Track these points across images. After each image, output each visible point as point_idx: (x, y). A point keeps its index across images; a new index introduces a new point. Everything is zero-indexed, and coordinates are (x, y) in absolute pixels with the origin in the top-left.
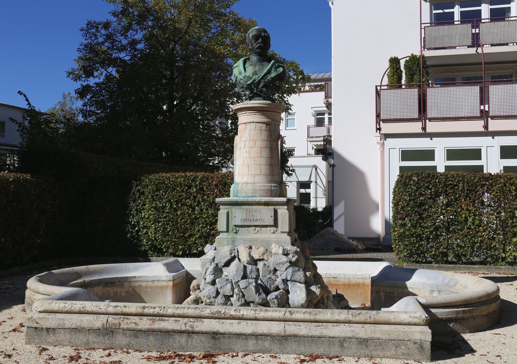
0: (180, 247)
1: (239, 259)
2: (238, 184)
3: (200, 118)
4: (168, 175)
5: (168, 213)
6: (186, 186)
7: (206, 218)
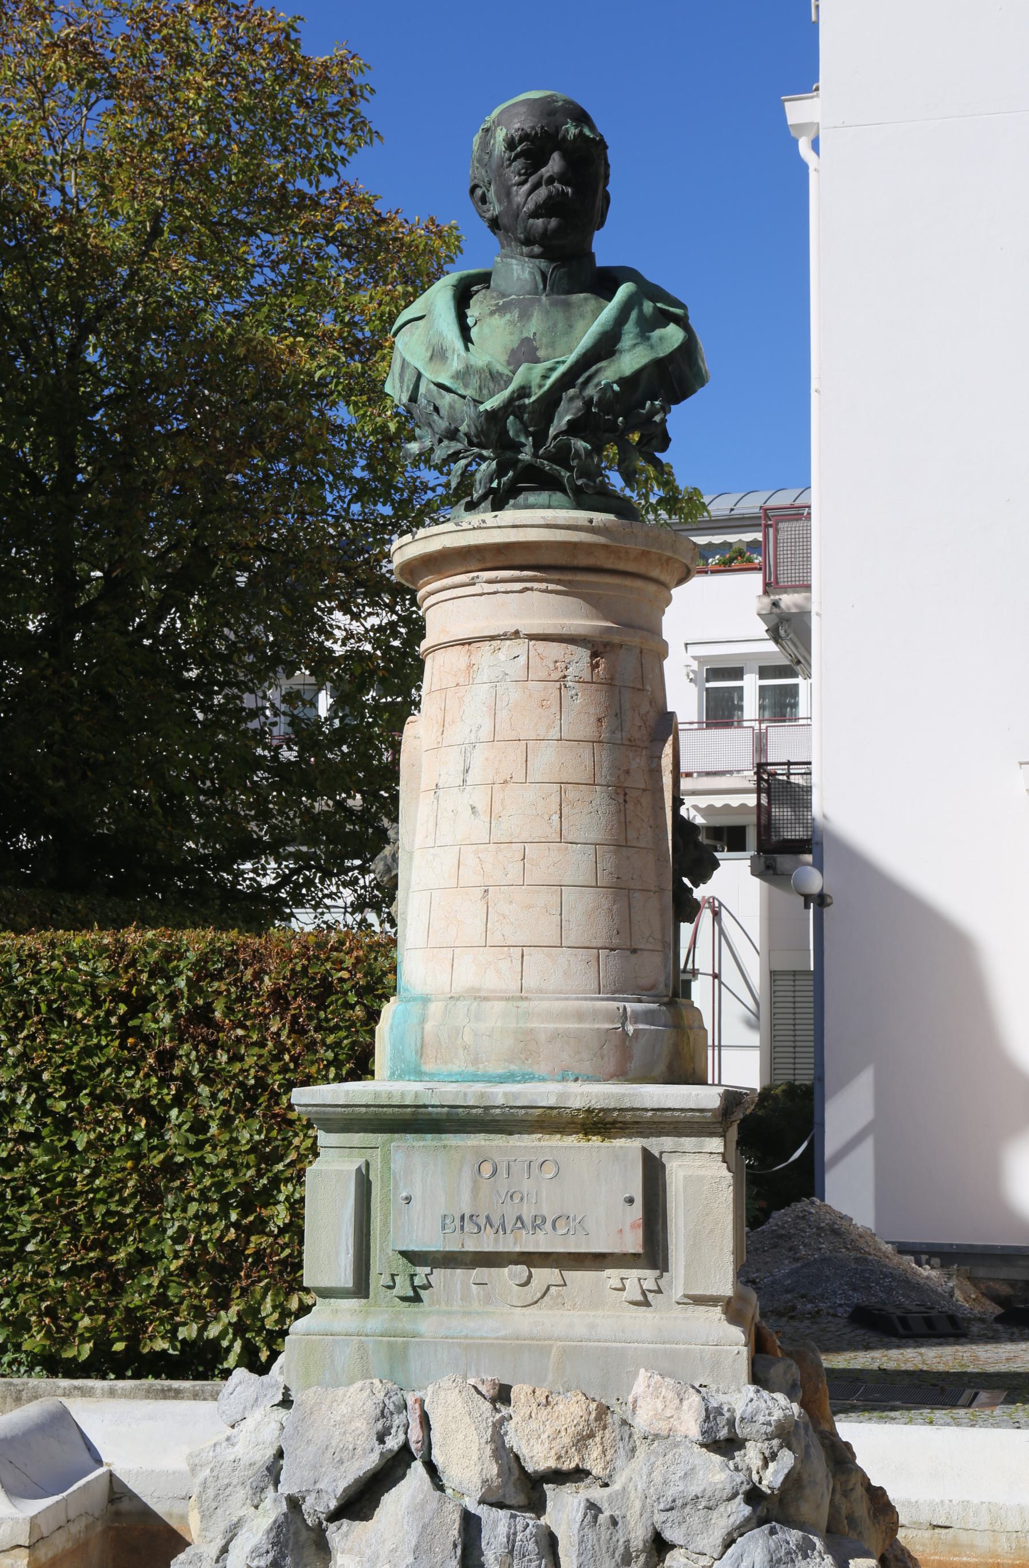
0: (86, 1322)
1: (431, 1468)
2: (425, 1000)
3: (193, 674)
4: (30, 942)
5: (23, 1137)
6: (119, 997)
7: (224, 1165)
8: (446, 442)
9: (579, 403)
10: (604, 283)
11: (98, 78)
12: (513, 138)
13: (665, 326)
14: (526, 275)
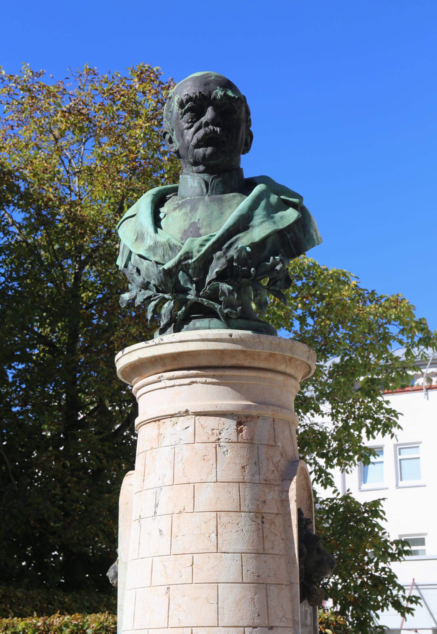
8: (143, 291)
9: (223, 260)
10: (246, 187)
11: (82, 124)
12: (182, 101)
13: (286, 209)
14: (196, 184)
